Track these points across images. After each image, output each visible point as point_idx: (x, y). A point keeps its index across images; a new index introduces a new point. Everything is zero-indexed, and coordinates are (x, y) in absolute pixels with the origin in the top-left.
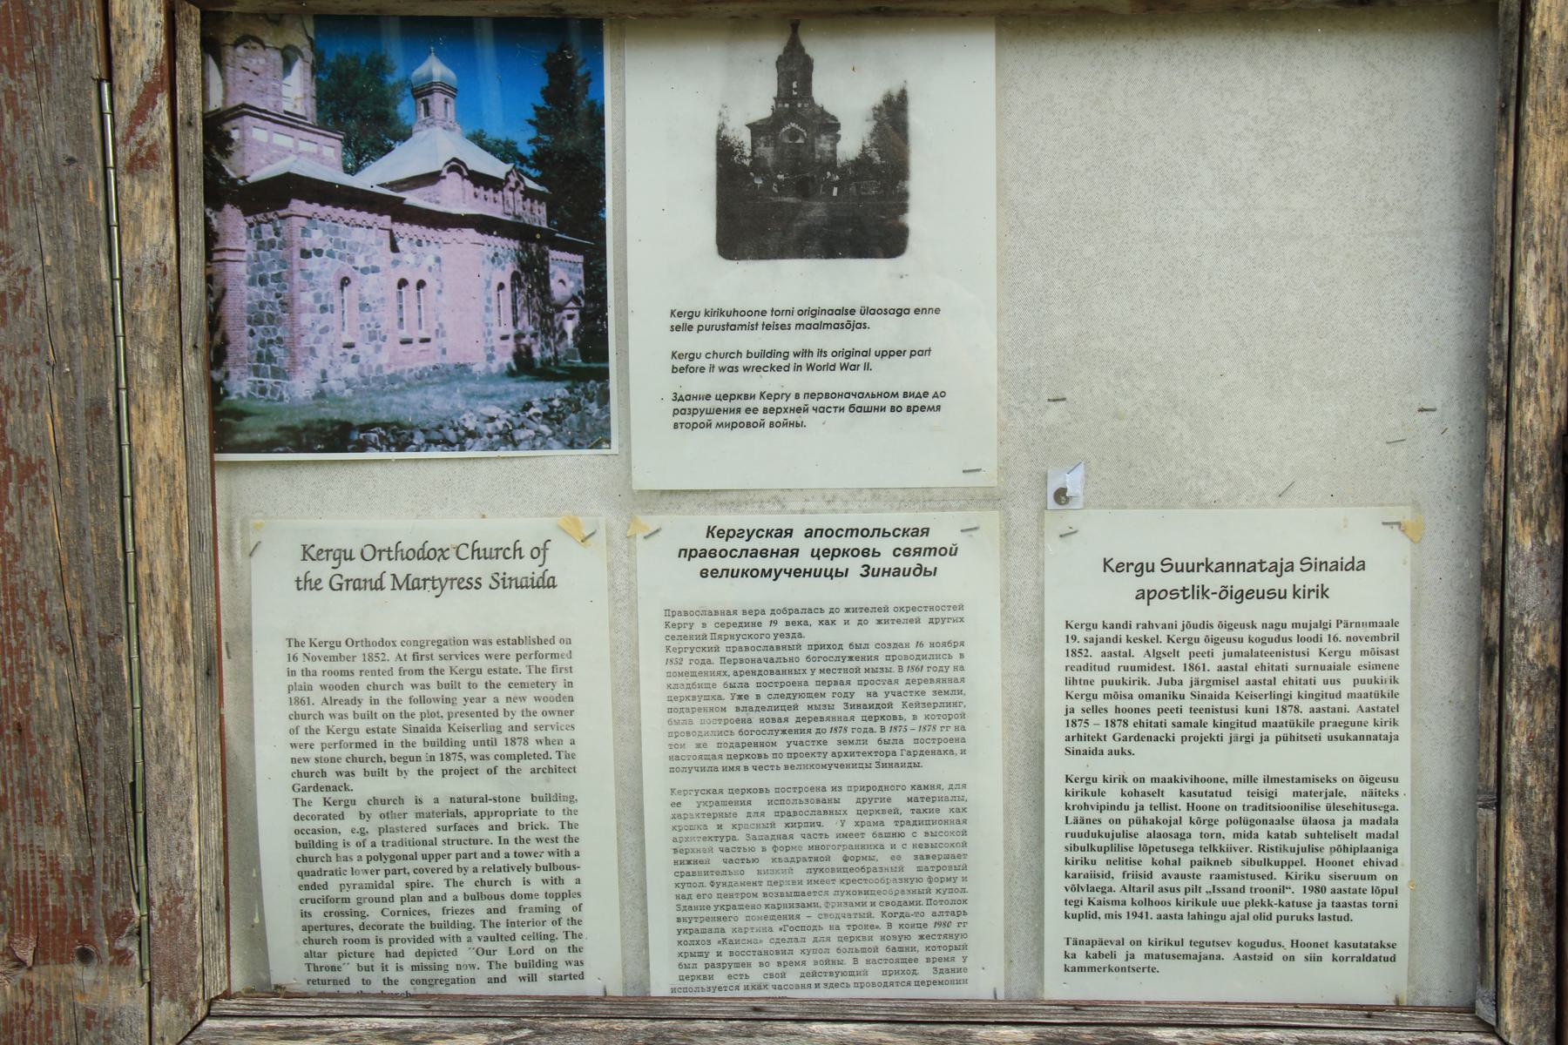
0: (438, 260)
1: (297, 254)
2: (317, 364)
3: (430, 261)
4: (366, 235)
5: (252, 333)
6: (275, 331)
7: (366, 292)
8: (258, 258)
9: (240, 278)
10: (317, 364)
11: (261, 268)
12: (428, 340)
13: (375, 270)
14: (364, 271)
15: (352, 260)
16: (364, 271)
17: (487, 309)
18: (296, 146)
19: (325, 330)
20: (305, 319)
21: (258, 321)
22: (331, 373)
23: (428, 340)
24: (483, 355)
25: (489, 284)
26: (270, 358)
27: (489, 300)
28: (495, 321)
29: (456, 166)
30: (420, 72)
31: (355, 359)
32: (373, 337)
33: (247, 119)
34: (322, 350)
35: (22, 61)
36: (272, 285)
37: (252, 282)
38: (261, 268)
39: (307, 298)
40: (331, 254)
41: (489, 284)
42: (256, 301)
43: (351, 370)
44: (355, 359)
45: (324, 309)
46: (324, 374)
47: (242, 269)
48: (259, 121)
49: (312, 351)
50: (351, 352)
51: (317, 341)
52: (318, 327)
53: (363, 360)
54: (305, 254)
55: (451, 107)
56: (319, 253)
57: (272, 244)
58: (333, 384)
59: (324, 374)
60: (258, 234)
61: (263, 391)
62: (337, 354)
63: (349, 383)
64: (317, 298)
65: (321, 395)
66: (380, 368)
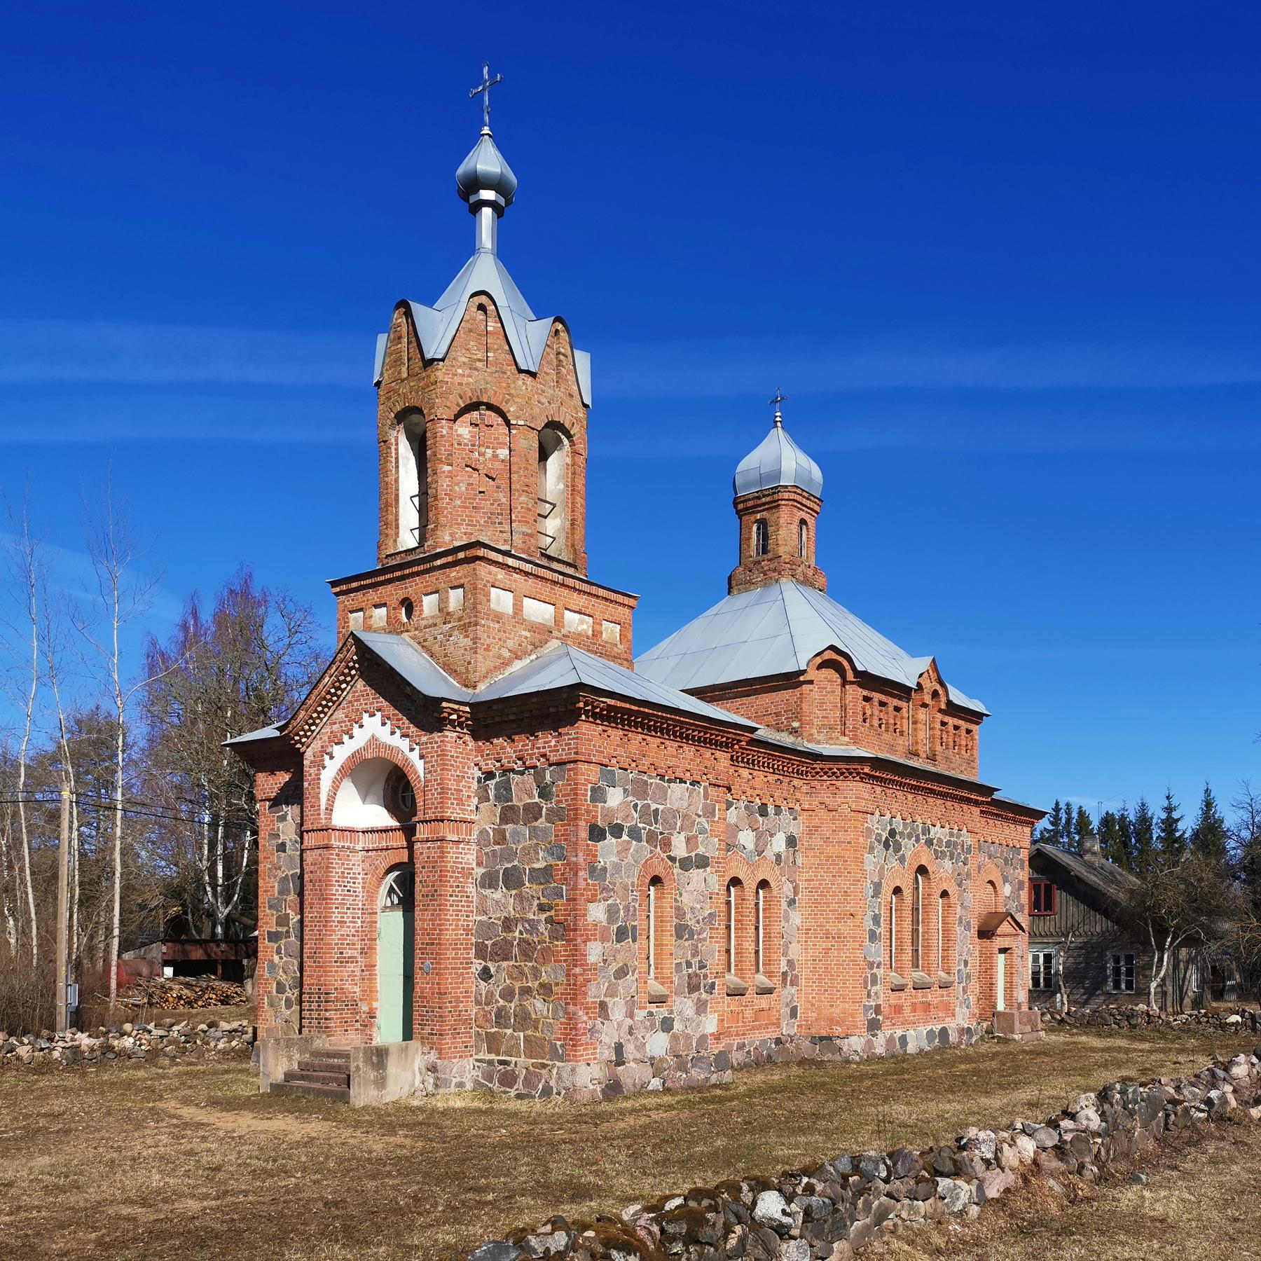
0: (791, 841)
1: (584, 834)
2: (609, 1034)
3: (778, 844)
4: (687, 794)
5: (486, 974)
6: (536, 973)
7: (686, 900)
8: (501, 837)
9: (467, 873)
10: (609, 1034)
11: (511, 855)
12: (769, 991)
13: (703, 862)
14: (685, 864)
15: (666, 844)
16: (685, 864)
17: (873, 936)
18: (559, 621)
19: (622, 973)
20: (594, 952)
21: (502, 952)
22: (630, 1051)
23: (769, 991)
24: (861, 1021)
25: (877, 887)
26: (524, 1020)
27: (876, 919)
28: (883, 957)
29: (835, 661)
30: (754, 462)
31: (667, 1025)
32: (693, 988)
33: (483, 569)
34: (618, 1012)
35: (1055, 822)
36: (529, 888)
37: (489, 881)
38: (511, 855)
39: (596, 913)
40: (635, 834)
41: (877, 887)
42: (496, 916)
43: (658, 1044)
44: (667, 1025)
45: (621, 934)
46: (619, 1048)
47: (468, 857)
48: (500, 574)
49: (603, 1006)
50: (661, 1012)
51: (612, 992)
52: (614, 967)
53: (677, 1026)
54: (597, 834)
55: (809, 535)
56: (617, 831)
57: (533, 812)
58: (633, 1073)
59: (619, 1048)
60: (504, 792)
61: (508, 1080)
62: (640, 1015)
63: (656, 1066)
64: (612, 913)
65: (613, 1089)
66: (703, 1039)
